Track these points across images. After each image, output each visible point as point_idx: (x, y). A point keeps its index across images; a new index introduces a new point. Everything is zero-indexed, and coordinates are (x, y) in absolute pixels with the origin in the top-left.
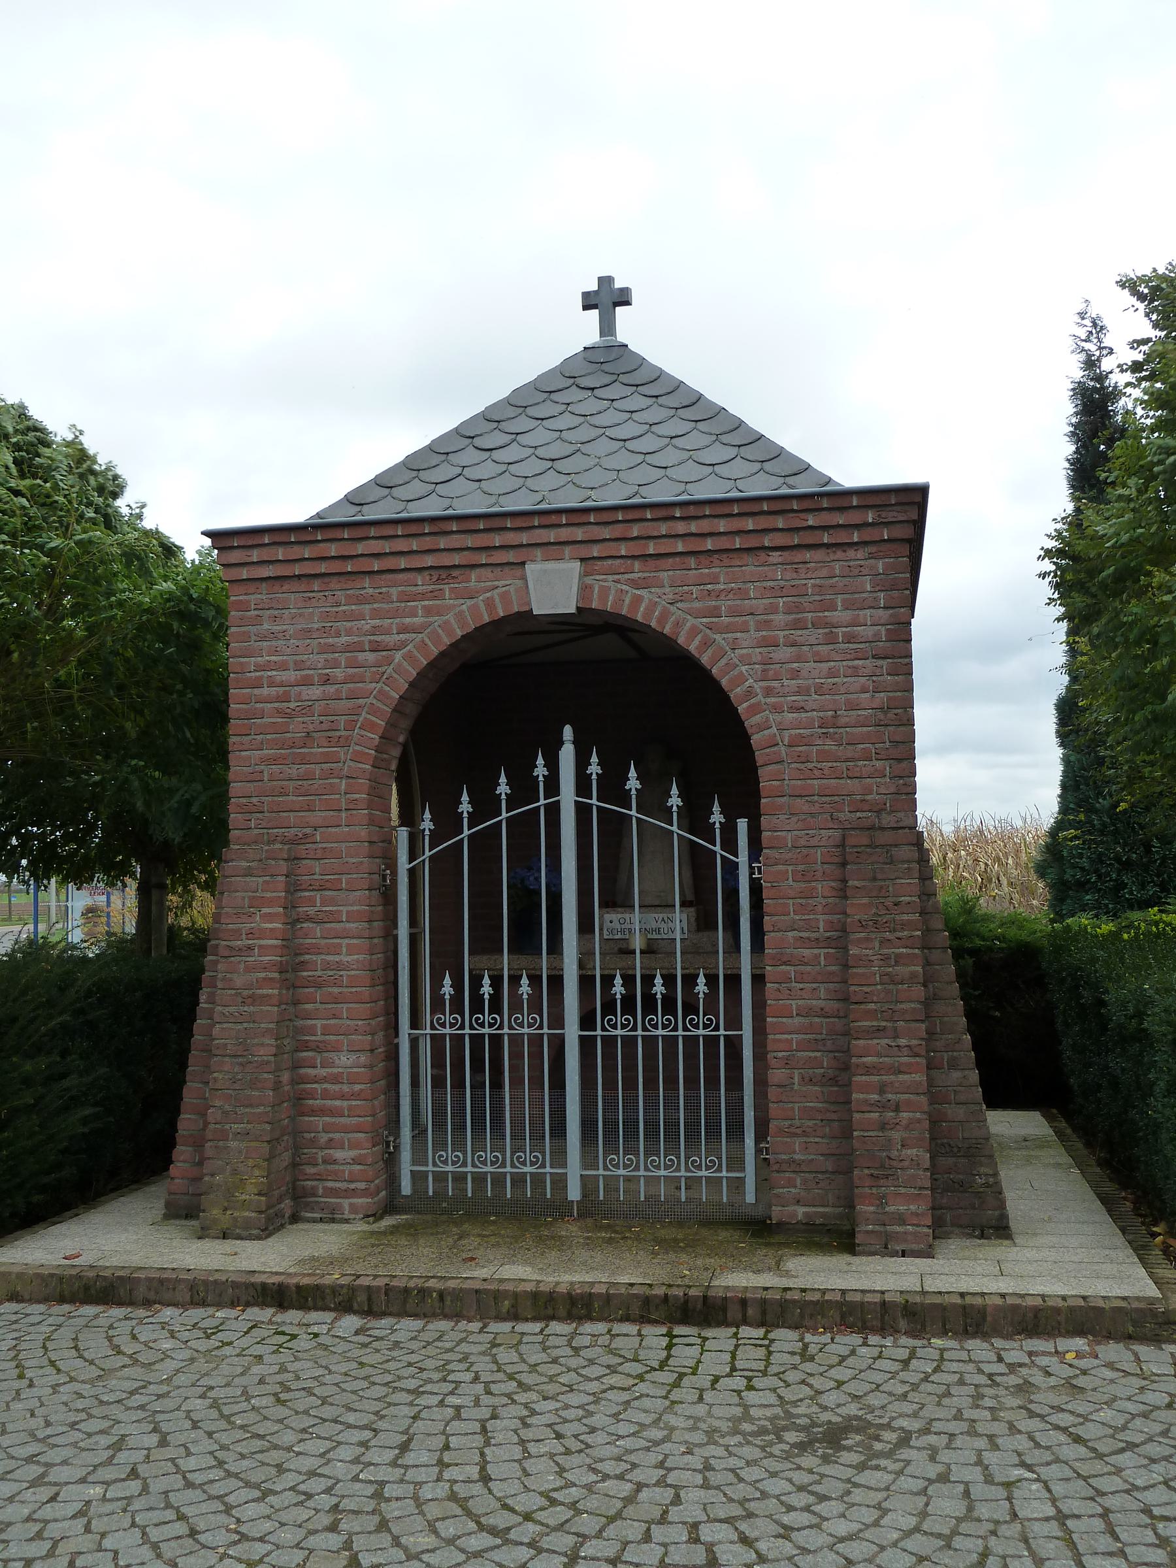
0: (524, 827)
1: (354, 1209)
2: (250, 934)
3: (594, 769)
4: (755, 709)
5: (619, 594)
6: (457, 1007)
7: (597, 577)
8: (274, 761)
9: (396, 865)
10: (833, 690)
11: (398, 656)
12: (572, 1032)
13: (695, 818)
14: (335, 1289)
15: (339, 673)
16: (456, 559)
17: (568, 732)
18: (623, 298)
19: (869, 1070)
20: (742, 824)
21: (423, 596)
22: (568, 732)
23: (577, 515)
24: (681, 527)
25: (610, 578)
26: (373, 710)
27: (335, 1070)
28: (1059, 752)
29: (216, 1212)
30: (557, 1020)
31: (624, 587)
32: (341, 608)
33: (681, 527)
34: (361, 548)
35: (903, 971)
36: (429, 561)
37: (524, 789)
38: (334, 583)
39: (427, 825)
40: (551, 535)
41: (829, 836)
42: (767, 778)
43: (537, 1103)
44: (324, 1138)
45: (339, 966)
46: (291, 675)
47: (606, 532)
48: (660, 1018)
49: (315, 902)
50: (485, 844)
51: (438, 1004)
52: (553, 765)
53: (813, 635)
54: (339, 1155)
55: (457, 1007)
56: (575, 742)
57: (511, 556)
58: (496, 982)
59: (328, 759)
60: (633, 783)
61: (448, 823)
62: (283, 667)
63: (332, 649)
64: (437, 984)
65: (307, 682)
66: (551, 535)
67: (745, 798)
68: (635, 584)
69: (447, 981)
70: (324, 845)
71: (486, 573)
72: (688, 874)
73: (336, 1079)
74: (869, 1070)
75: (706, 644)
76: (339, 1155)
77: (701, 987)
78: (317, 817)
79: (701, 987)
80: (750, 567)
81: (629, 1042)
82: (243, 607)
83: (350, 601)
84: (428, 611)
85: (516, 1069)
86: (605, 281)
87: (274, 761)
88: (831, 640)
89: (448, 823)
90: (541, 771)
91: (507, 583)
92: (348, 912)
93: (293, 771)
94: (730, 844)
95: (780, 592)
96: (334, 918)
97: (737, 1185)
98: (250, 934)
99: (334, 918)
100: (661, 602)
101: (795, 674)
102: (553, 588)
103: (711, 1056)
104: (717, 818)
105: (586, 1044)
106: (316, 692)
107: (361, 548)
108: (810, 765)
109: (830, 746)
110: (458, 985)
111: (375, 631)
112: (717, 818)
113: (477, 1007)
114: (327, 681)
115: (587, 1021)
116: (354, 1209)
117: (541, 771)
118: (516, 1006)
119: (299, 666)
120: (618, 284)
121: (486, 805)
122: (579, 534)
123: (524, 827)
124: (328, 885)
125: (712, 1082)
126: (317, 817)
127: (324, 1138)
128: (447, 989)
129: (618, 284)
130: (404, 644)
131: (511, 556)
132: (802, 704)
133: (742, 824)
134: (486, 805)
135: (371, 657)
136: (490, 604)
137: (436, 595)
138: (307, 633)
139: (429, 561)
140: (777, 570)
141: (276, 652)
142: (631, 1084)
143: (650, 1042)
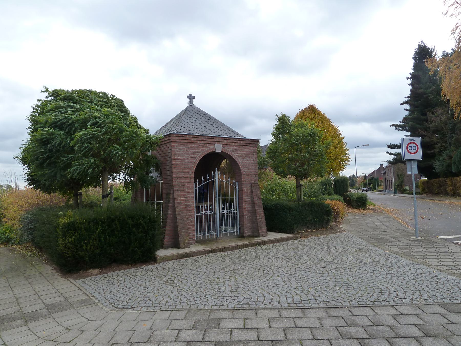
0: (211, 183)
1: (193, 243)
2: (180, 200)
3: (220, 174)
4: (242, 167)
8: (180, 172)
10: (250, 165)
14: (218, 249)
15: (189, 158)
18: (194, 98)
19: (258, 214)
21: (201, 147)
23: (223, 138)
24: (234, 141)
26: (194, 164)
29: (182, 245)
33: (234, 141)
34: (193, 139)
35: (260, 202)
36: (202, 142)
38: (188, 144)
39: (197, 182)
40: (219, 140)
41: (249, 185)
43: (232, 221)
45: (190, 205)
46: (182, 158)
47: (225, 141)
48: (211, 211)
52: (214, 174)
53: (247, 158)
54: (191, 234)
57: (213, 143)
58: (202, 207)
59: (188, 172)
61: (200, 183)
62: (180, 156)
63: (188, 154)
64: (231, 205)
65: (184, 159)
66: (219, 140)
68: (228, 149)
73: (190, 223)
74: (258, 214)
75: (236, 158)
76: (191, 234)
77: (201, 208)
78: (186, 181)
79: (201, 208)
80: (241, 148)
82: (174, 146)
83: (191, 147)
84: (202, 150)
85: (205, 218)
86: (191, 95)
87: (180, 172)
88: (249, 158)
90: (213, 175)
91: (212, 147)
93: (183, 173)
95: (244, 151)
96: (189, 197)
97: (216, 235)
98: (180, 200)
99: (189, 197)
100: (230, 151)
101: (246, 163)
102: (219, 148)
106: (186, 161)
107: (193, 139)
109: (249, 172)
111: (194, 152)
112: (234, 182)
114: (187, 159)
116: (193, 243)
119: (183, 157)
120: (193, 95)
122: (222, 141)
126: (186, 181)
129: (193, 95)
131: (213, 143)
134: (206, 180)
135: (194, 156)
136: (210, 149)
137: (203, 147)
138: (184, 151)
139: (202, 142)
141: (179, 154)
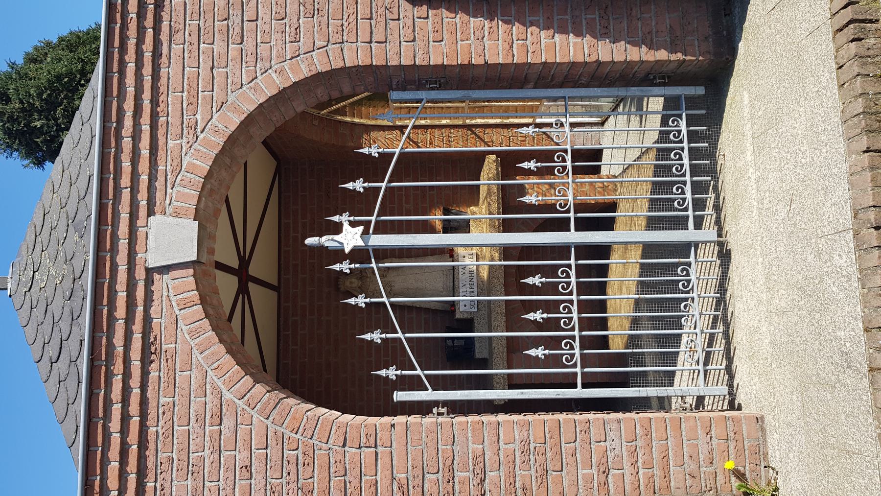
5: (183, 187)
7: (167, 202)
9: (430, 401)
11: (227, 396)
16: (137, 338)
17: (310, 241)
20: (400, 396)
22: (310, 241)
25: (169, 191)
27: (625, 454)
30: (562, 251)
31: (179, 178)
32: (175, 457)
49: (464, 477)
51: (555, 361)
55: (555, 343)
56: (321, 236)
60: (358, 185)
64: (536, 362)
69: (532, 352)
70: (410, 468)
71: (154, 311)
72: (431, 258)
78: (383, 478)
92: (474, 443)
108: (346, 24)
110: (536, 343)
117: (345, 267)
124: (449, 462)
128: (539, 352)
130: (215, 387)
132: (293, 29)
133: (400, 396)
139: (136, 364)
140: (174, 52)
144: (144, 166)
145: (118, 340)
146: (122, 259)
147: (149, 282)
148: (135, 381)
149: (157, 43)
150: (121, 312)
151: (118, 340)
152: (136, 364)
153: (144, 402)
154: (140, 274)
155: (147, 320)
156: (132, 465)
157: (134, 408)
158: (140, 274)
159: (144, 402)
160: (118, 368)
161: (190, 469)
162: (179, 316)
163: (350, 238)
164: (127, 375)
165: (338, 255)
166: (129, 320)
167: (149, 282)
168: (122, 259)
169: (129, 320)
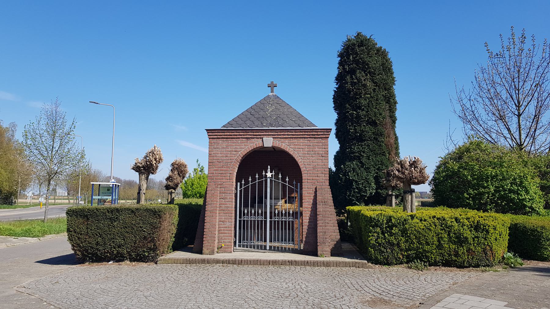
6: (255, 215)
12: (268, 220)
13: (283, 179)
20: (299, 184)
28: (339, 145)
30: (266, 218)
37: (261, 176)
42: (304, 176)
44: (223, 238)
50: (253, 186)
60: (287, 179)
67: (299, 179)
75: (293, 153)
81: (278, 221)
89: (247, 182)
94: (297, 187)
102: (269, 142)
103: (278, 223)
104: (294, 183)
105: (271, 222)
112: (294, 183)
113: (251, 215)
115: (271, 218)
117: (264, 173)
118: (244, 215)
121: (254, 179)
123: (260, 183)
125: (285, 229)
127: (223, 238)
133: (299, 184)
134: (254, 179)
139: (246, 136)
142: (285, 229)
143: (251, 221)
144: (282, 136)
145: (250, 133)
146: (265, 133)
147: (261, 138)
148: (243, 136)
149: (307, 138)
150: (255, 134)
151: (250, 133)
152: (246, 136)
153: (239, 138)
154: (262, 137)
155: (254, 138)
156: (228, 137)
157: (238, 136)
158: (262, 137)
159: (239, 138)
160: (245, 134)
161: (227, 146)
162: (255, 144)
163: (269, 175)
164: (244, 135)
165: (266, 172)
166: (253, 135)
167: (261, 138)
168: (265, 133)
169: (253, 135)
